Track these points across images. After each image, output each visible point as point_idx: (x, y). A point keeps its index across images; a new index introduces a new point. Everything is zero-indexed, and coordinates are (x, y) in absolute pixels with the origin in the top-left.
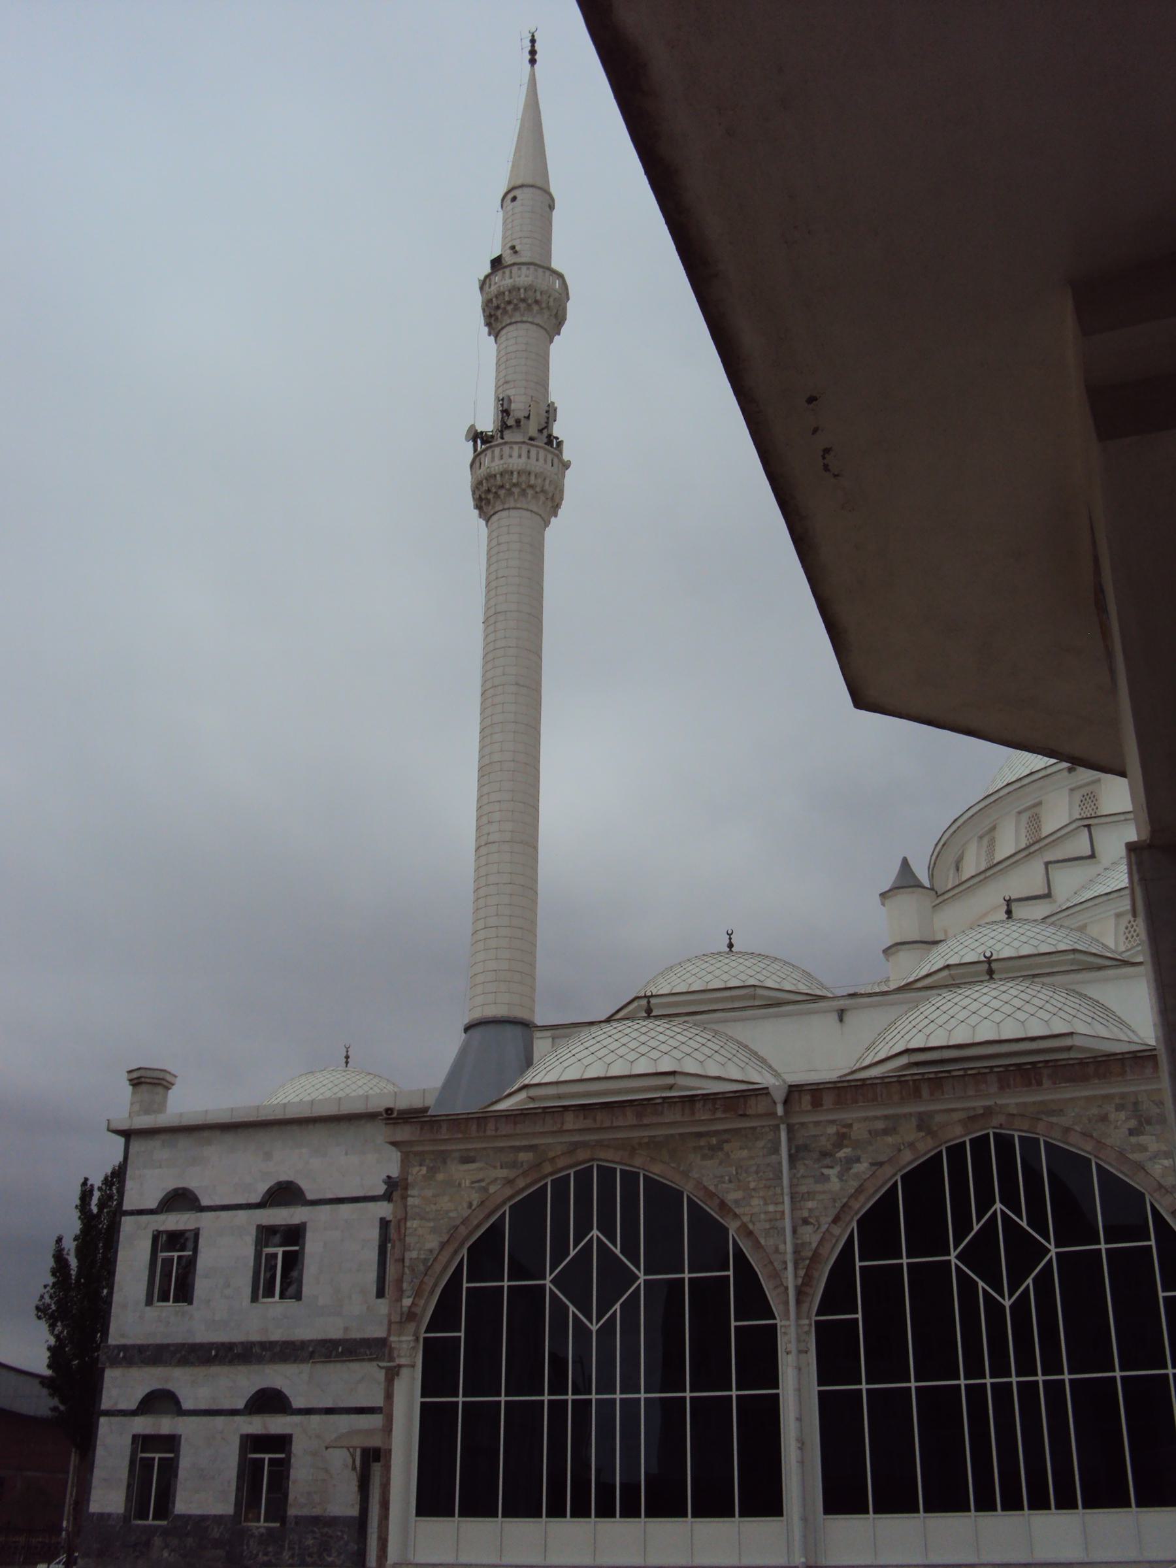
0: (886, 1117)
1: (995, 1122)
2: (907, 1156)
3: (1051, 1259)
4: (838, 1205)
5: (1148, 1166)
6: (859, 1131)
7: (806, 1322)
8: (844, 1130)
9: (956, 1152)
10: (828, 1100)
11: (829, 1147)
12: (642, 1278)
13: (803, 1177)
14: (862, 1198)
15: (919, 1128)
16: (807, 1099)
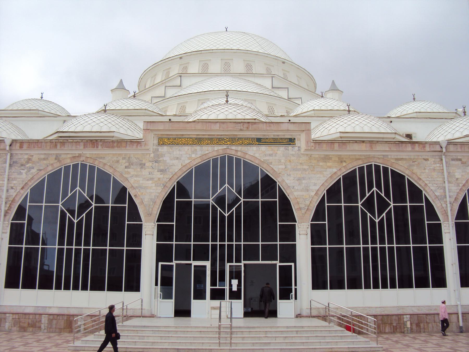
0: (45, 154)
1: (81, 160)
2: (50, 168)
3: (391, 208)
4: (24, 183)
5: (129, 179)
6: (35, 158)
7: (7, 223)
8: (30, 157)
9: (67, 168)
10: (25, 146)
11: (24, 163)
12: (94, 205)
13: (14, 172)
14: (32, 181)
15: (56, 159)
16: (18, 145)
